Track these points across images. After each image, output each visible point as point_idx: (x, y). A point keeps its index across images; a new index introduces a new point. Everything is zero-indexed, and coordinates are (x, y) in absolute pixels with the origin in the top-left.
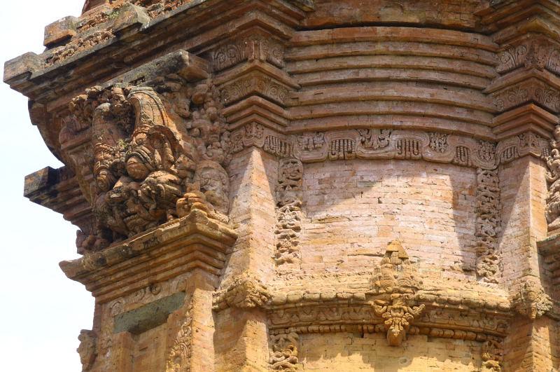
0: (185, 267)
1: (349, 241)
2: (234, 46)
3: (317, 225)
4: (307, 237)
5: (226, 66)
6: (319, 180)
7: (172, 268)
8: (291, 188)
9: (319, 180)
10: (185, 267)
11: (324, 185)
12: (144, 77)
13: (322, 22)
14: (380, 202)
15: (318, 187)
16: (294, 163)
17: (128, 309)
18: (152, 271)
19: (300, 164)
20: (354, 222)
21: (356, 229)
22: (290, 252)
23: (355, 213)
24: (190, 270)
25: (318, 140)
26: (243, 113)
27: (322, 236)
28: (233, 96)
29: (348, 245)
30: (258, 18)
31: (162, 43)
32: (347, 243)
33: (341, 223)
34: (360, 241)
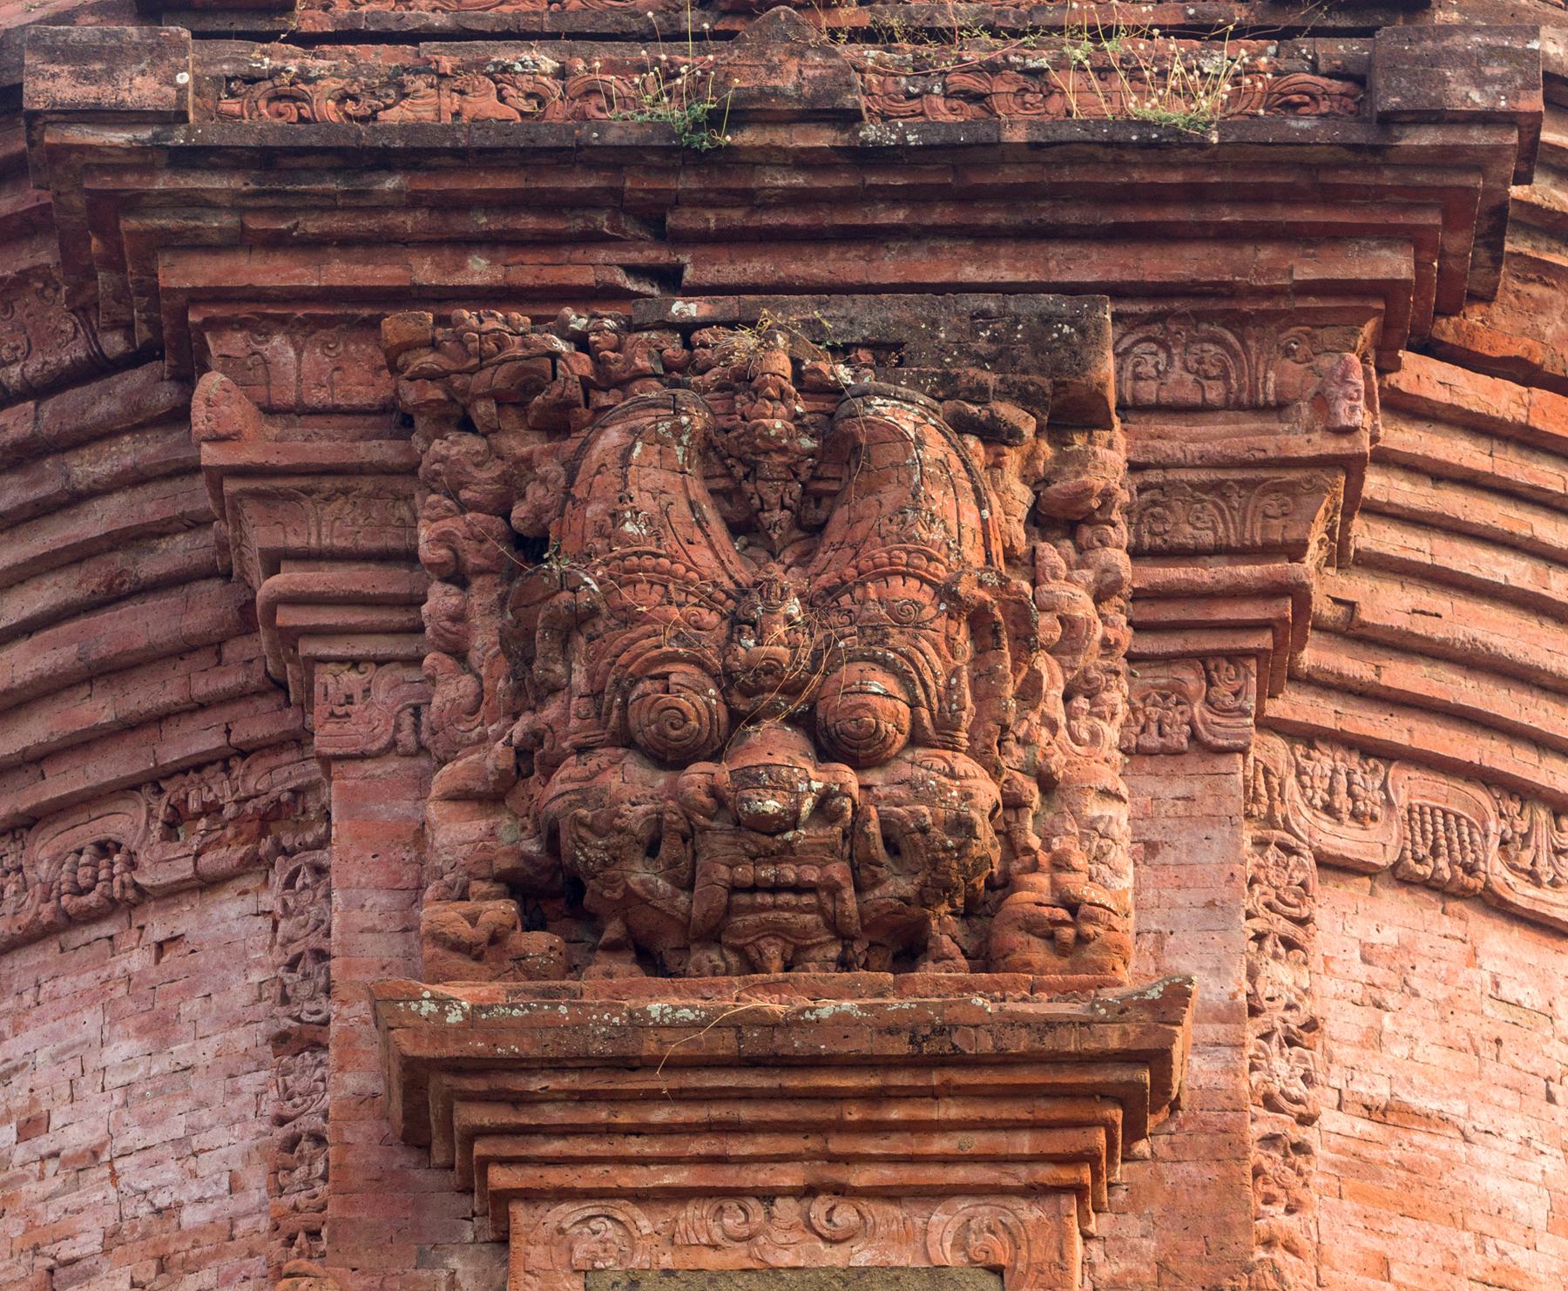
0: (1023, 1175)
1: (1470, 1224)
2: (1230, 337)
3: (1363, 1127)
4: (1334, 1165)
5: (1165, 396)
6: (1363, 945)
7: (946, 1160)
8: (1281, 950)
9: (1363, 945)
10: (1023, 1175)
11: (1379, 974)
12: (898, 346)
13: (1503, 349)
14: (1550, 1098)
15: (1361, 971)
16: (1289, 850)
17: (666, 1261)
18: (837, 1145)
19: (1310, 862)
20: (1478, 1152)
21: (1489, 1183)
22: (1290, 1211)
23: (1483, 1118)
24: (1033, 1192)
25: (1368, 781)
26: (1224, 613)
27: (1380, 1176)
28: (1189, 529)
29: (1468, 1239)
30: (1237, 253)
31: (899, 216)
32: (1464, 1228)
33: (1442, 1145)
34: (1505, 1234)
